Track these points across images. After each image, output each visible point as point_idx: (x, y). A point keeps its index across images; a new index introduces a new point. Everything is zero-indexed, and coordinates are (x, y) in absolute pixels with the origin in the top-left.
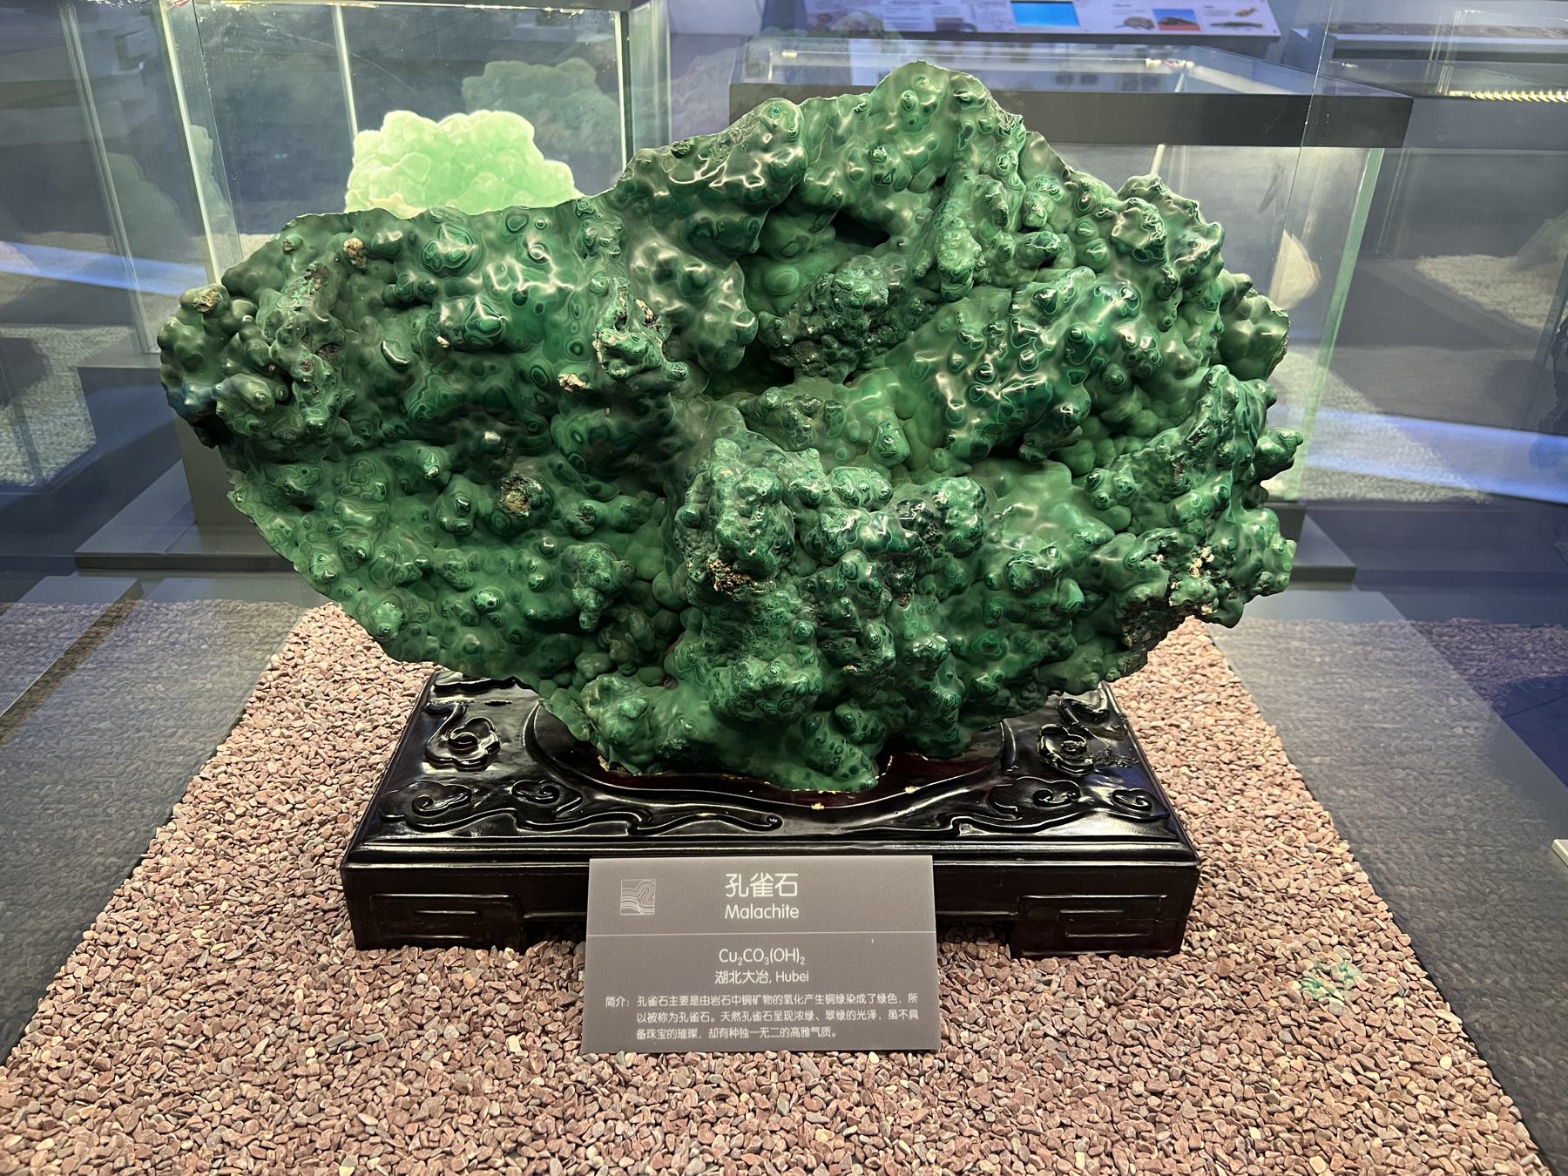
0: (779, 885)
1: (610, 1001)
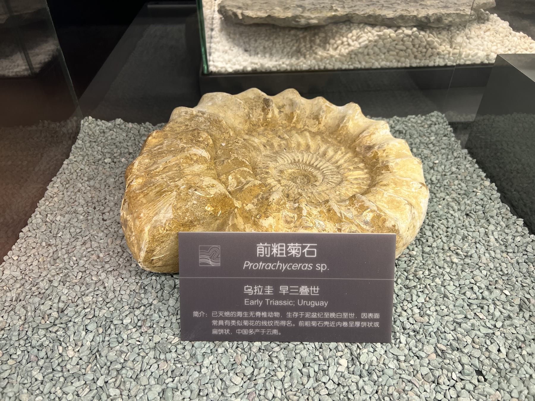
0: (305, 250)
1: (196, 314)
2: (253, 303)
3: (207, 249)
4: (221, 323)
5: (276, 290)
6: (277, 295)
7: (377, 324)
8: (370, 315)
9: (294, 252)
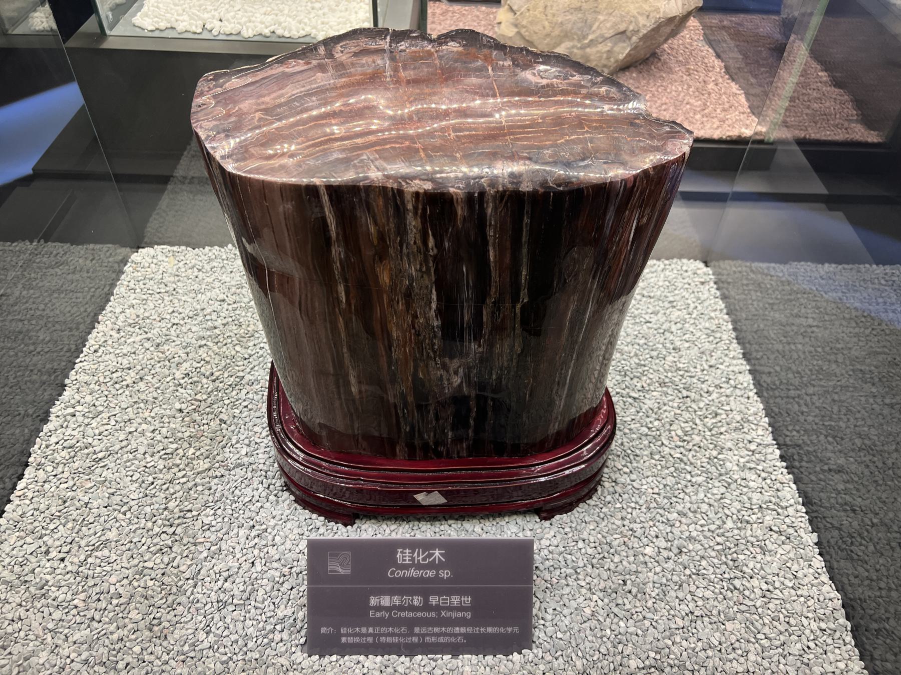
1: (324, 630)
5: (426, 600)
6: (427, 607)
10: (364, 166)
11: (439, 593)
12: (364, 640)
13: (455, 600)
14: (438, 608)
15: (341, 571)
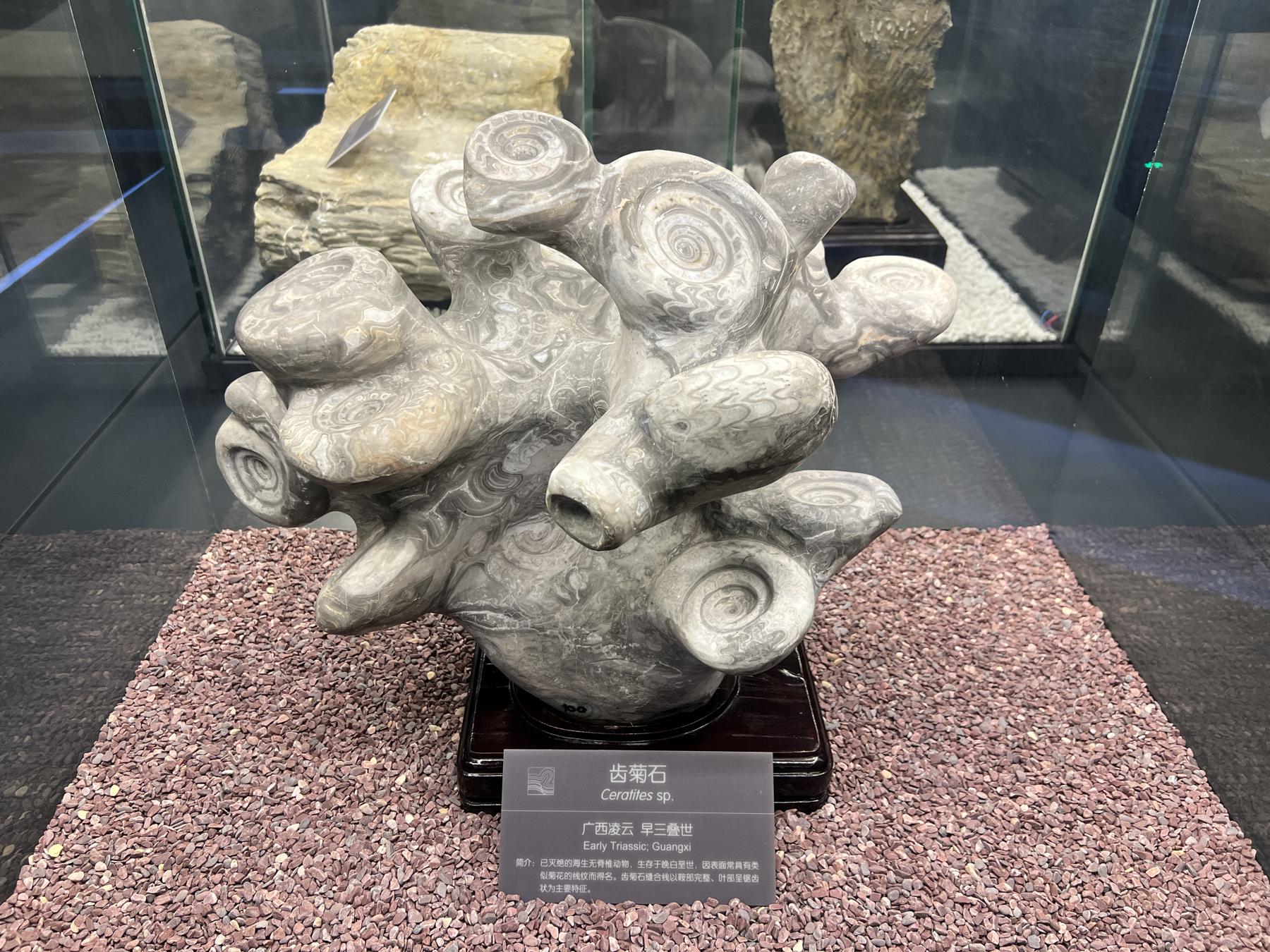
0: (652, 774)
1: (520, 862)
2: (594, 847)
3: (537, 771)
4: (552, 875)
5: (637, 829)
6: (638, 837)
7: (756, 879)
8: (714, 864)
9: (637, 776)
10: (819, 281)
11: (653, 819)
12: (650, 863)
13: (673, 829)
14: (649, 840)
15: (544, 792)
